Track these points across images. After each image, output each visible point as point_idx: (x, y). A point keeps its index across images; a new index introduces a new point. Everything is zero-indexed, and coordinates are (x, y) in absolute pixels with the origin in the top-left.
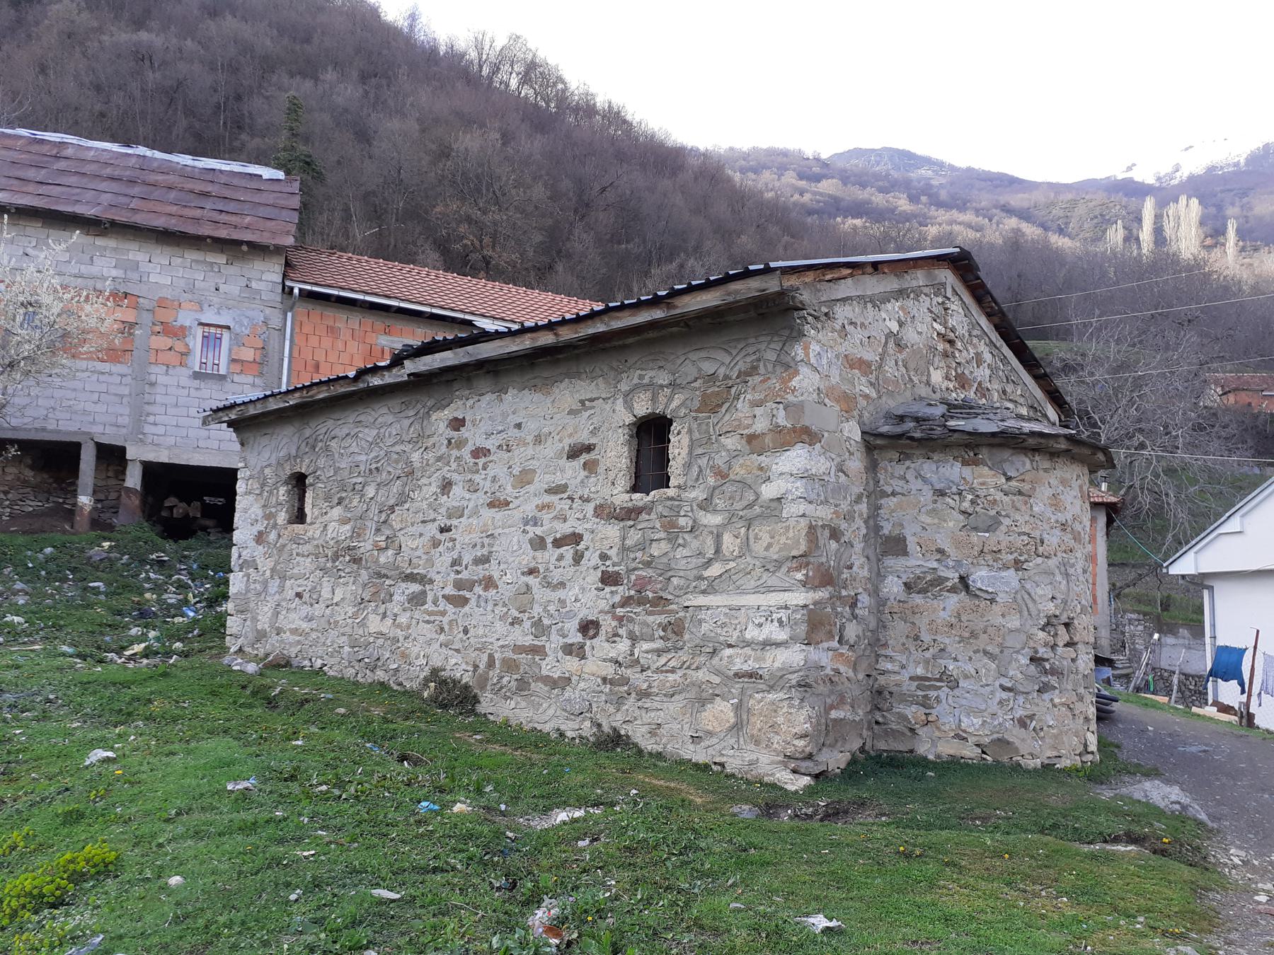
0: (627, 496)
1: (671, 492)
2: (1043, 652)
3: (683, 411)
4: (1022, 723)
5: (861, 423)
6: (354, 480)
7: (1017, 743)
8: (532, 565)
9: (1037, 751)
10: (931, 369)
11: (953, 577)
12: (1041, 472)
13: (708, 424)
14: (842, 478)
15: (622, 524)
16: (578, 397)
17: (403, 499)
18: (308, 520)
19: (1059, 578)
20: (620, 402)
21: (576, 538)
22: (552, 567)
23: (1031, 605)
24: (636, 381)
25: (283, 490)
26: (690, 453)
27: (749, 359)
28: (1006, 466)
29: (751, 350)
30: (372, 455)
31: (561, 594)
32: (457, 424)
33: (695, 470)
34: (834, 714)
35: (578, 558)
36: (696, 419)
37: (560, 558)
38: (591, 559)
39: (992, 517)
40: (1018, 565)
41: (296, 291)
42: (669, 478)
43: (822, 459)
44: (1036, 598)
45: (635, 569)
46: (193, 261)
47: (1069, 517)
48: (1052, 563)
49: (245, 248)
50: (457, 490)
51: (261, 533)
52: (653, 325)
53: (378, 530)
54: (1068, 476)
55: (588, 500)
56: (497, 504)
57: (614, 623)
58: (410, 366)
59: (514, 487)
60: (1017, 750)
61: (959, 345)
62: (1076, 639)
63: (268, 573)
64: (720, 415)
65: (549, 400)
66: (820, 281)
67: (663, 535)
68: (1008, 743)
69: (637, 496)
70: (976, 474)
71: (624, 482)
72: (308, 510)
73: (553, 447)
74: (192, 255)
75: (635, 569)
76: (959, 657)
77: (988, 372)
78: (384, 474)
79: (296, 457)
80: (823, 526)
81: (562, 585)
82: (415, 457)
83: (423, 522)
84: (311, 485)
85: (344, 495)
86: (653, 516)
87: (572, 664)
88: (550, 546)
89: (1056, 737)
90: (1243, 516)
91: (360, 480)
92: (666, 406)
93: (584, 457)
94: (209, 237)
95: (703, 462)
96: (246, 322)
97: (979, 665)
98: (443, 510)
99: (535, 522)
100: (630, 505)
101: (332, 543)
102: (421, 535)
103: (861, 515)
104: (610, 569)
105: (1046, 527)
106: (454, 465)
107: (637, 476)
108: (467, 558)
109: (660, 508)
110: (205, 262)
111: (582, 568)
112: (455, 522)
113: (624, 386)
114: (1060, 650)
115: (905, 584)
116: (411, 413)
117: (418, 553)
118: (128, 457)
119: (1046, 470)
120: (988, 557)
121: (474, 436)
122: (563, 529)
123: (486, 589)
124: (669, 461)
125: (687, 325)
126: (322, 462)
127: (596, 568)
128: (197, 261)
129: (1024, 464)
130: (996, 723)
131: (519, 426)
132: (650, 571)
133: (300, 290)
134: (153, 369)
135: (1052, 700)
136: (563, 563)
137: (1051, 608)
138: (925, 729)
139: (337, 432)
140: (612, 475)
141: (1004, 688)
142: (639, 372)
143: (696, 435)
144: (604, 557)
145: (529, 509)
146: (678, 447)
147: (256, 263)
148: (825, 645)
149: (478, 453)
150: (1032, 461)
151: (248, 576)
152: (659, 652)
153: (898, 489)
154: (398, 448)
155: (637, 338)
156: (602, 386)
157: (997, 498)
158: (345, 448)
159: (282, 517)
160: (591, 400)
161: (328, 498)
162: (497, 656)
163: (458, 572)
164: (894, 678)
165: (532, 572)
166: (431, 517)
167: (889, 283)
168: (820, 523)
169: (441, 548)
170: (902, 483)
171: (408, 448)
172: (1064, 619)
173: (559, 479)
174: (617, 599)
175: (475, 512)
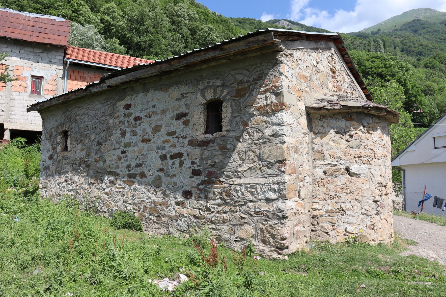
0: (203, 136)
1: (223, 133)
2: (378, 198)
3: (228, 97)
5: (305, 103)
6: (86, 132)
8: (161, 167)
13: (240, 102)
15: (201, 148)
16: (180, 92)
17: (106, 139)
18: (69, 150)
19: (382, 167)
20: (199, 94)
21: (180, 155)
22: (170, 168)
24: (206, 84)
25: (59, 137)
26: (232, 115)
27: (257, 74)
28: (363, 121)
29: (258, 69)
30: (93, 122)
31: (174, 179)
32: (128, 107)
33: (235, 123)
35: (181, 164)
36: (234, 100)
37: (173, 164)
38: (187, 163)
41: (69, 62)
42: (222, 127)
43: (291, 117)
44: (375, 176)
45: (207, 168)
46: (28, 51)
47: (385, 142)
48: (380, 161)
49: (48, 46)
50: (128, 135)
51: (51, 155)
52: (214, 59)
53: (96, 153)
54: (384, 126)
55: (184, 138)
56: (146, 141)
57: (198, 192)
58: (108, 83)
59: (152, 133)
61: (337, 73)
62: (388, 192)
63: (54, 172)
64: (245, 98)
65: (168, 94)
66: (287, 40)
67: (220, 153)
68: (365, 236)
69: (208, 135)
70: (351, 124)
71: (202, 130)
72: (69, 145)
73: (169, 115)
74: (28, 49)
75: (207, 168)
76: (346, 202)
77: (347, 85)
78: (98, 129)
79: (63, 124)
80: (292, 147)
81: (174, 176)
82: (111, 121)
83: (114, 149)
84: (70, 135)
85: (82, 139)
86: (215, 144)
87: (180, 210)
88: (168, 159)
90: (415, 145)
91: (88, 132)
92: (221, 95)
93: (184, 119)
94: (34, 42)
95: (238, 119)
96: (49, 75)
97: (353, 204)
98: (122, 144)
99: (163, 148)
100: (204, 140)
101: (78, 159)
102: (114, 155)
104: (196, 168)
105: (378, 146)
106: (126, 124)
107: (207, 127)
108: (133, 164)
109: (218, 141)
110: (33, 52)
111: (184, 168)
112: (127, 149)
113: (201, 87)
116: (109, 103)
117: (113, 162)
118: (5, 127)
119: (377, 123)
120: (357, 159)
121: (135, 112)
122: (174, 151)
123: (141, 177)
124: (222, 119)
125: (229, 59)
126: (73, 125)
127: (189, 168)
128: (30, 52)
129: (369, 120)
130: (360, 228)
131: (154, 106)
132: (214, 169)
133: (70, 62)
134: (14, 93)
135: (380, 217)
136: (174, 166)
138: (332, 232)
139: (79, 112)
140: (196, 126)
142: (208, 80)
143: (235, 107)
144: (193, 163)
145: (159, 142)
146: (226, 113)
147: (53, 52)
148: (293, 199)
149: (137, 119)
150: (372, 119)
151: (46, 173)
152: (219, 205)
153: (320, 131)
154: (103, 118)
155: (207, 66)
156: (191, 87)
158: (82, 119)
159: (59, 149)
160: (186, 94)
161: (76, 141)
162: (148, 206)
163: (129, 171)
164: (321, 211)
165: (161, 170)
166: (118, 147)
168: (291, 146)
169: (122, 161)
170: (322, 128)
171: (108, 118)
173: (172, 129)
174: (199, 182)
175: (136, 145)
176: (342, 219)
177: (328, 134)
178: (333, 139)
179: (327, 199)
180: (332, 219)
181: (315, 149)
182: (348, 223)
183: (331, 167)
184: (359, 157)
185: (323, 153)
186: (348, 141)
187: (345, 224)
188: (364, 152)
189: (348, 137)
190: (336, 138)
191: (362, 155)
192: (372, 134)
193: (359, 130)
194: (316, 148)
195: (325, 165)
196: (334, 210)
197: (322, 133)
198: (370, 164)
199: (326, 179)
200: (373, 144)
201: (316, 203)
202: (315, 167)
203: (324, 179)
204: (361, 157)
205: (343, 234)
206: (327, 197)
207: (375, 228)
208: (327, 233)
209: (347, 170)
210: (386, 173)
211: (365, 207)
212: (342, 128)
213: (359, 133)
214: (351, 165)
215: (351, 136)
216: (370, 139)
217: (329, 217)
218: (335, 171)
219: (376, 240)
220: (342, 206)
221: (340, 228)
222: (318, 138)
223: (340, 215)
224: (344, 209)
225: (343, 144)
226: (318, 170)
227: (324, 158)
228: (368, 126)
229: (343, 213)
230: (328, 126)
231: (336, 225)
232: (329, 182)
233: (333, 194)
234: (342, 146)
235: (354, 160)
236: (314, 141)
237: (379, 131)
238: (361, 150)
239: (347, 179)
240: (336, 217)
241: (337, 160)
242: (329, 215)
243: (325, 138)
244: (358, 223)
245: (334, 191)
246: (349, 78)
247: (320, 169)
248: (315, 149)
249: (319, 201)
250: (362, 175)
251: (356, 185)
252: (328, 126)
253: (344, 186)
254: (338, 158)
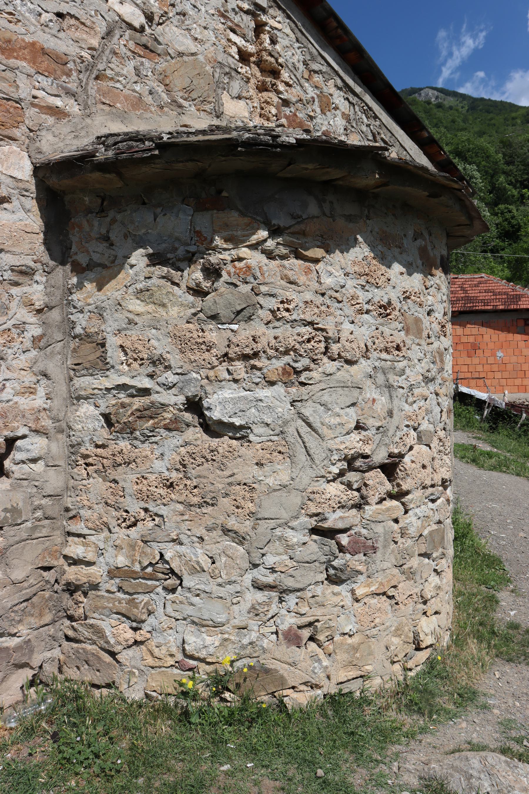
2: (334, 520)
4: (292, 638)
7: (283, 669)
9: (320, 678)
10: (225, 97)
11: (175, 399)
12: (341, 222)
23: (312, 441)
39: (247, 297)
40: (292, 375)
44: (324, 431)
60: (282, 682)
61: (285, 75)
62: (405, 487)
68: (267, 671)
89: (355, 649)
97: (215, 550)
105: (350, 311)
114: (369, 510)
115: (106, 417)
119: (350, 218)
120: (239, 366)
130: (246, 641)
135: (353, 592)
137: (354, 443)
138: (130, 652)
141: (259, 587)
153: (96, 257)
157: (252, 262)
164: (92, 569)
170: (102, 247)
172: (380, 456)
176: (168, 604)
177: (121, 267)
178: (140, 286)
179: (113, 523)
180: (132, 602)
181: (78, 330)
182: (193, 622)
183: (127, 400)
184: (245, 357)
185: (103, 345)
186: (198, 292)
187: (181, 626)
188: (271, 333)
189: (199, 275)
190: (150, 282)
191: (259, 347)
192: (316, 261)
193: (253, 247)
194: (82, 322)
195: (108, 390)
196: (137, 568)
197: (104, 266)
198: (303, 384)
199: (113, 447)
200: (319, 299)
201: (79, 535)
202: (79, 398)
203: (103, 446)
204: (256, 355)
205: (171, 661)
206: (112, 517)
207: (321, 637)
208: (113, 654)
209: (194, 406)
210: (390, 414)
211: (270, 560)
212: (178, 239)
213: (253, 259)
214: (209, 389)
215: (213, 272)
216: (302, 279)
217: (120, 595)
218: (143, 414)
219: (324, 682)
220: (167, 557)
221: (161, 640)
222: (90, 287)
223: (160, 590)
224: (174, 565)
225: (179, 305)
226: (86, 409)
227: (103, 365)
228: (297, 228)
229: (172, 582)
230: (126, 237)
231: (146, 627)
232: (119, 460)
233: (135, 507)
234: (174, 311)
235: (222, 371)
236: (74, 297)
237: (361, 252)
238: (257, 328)
239: (189, 448)
240: (145, 598)
241: (151, 369)
242: (120, 589)
243: (113, 283)
244: (237, 622)
245: (141, 496)
246: (354, 100)
247: (92, 408)
248: (78, 330)
249: (86, 531)
250: (258, 430)
251: (227, 473)
252: (126, 237)
253: (174, 476)
254: (154, 363)
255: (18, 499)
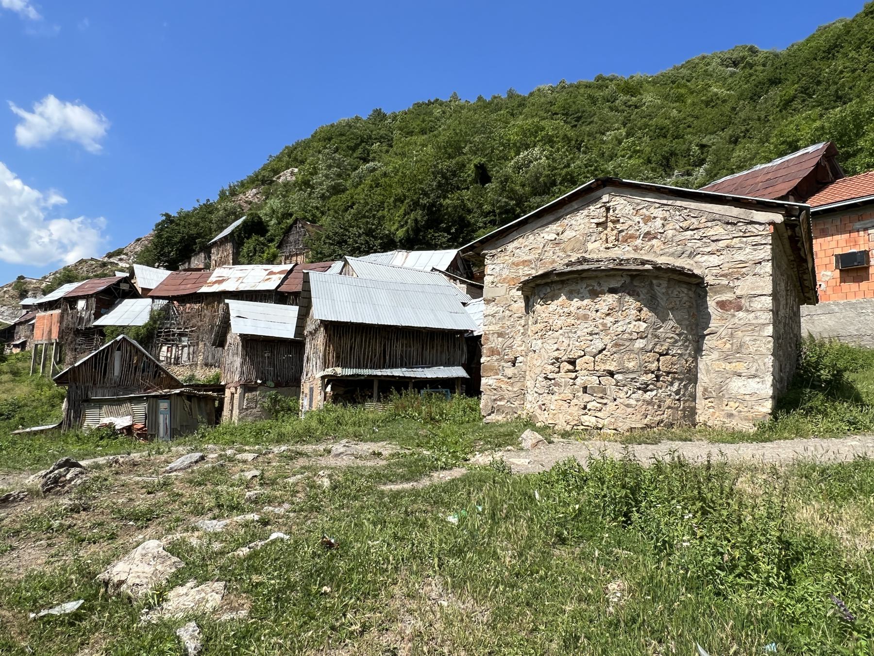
14: (507, 313)
34: (499, 403)
61: (621, 221)
103: (520, 325)
137: (556, 354)
167: (551, 218)
255: (516, 371)
